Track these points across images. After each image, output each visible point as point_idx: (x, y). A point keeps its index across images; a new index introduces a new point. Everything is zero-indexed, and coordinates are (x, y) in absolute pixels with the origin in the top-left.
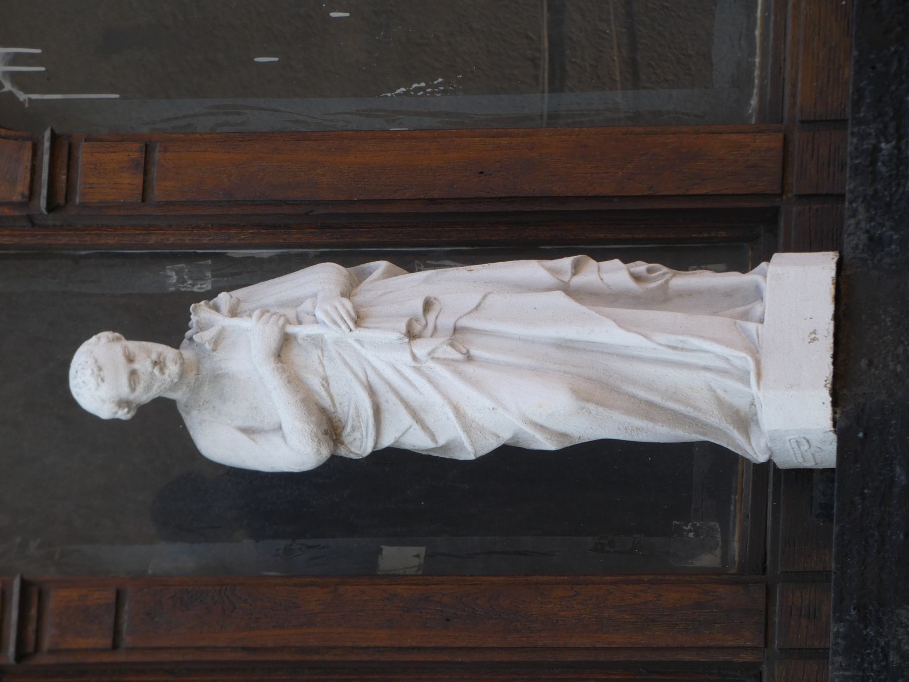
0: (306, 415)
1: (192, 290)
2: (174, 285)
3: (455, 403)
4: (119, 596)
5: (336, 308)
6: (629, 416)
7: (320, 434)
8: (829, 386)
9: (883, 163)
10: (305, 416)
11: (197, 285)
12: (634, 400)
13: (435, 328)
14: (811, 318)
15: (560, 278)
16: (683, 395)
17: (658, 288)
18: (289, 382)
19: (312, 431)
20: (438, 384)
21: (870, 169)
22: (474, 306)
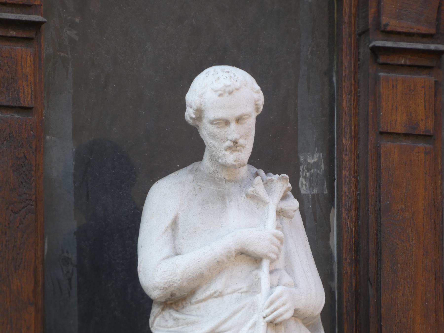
1: (301, 176)
2: (305, 160)
4: (27, 109)
5: (284, 304)
7: (170, 290)
11: (305, 181)
18: (218, 262)
19: (174, 282)
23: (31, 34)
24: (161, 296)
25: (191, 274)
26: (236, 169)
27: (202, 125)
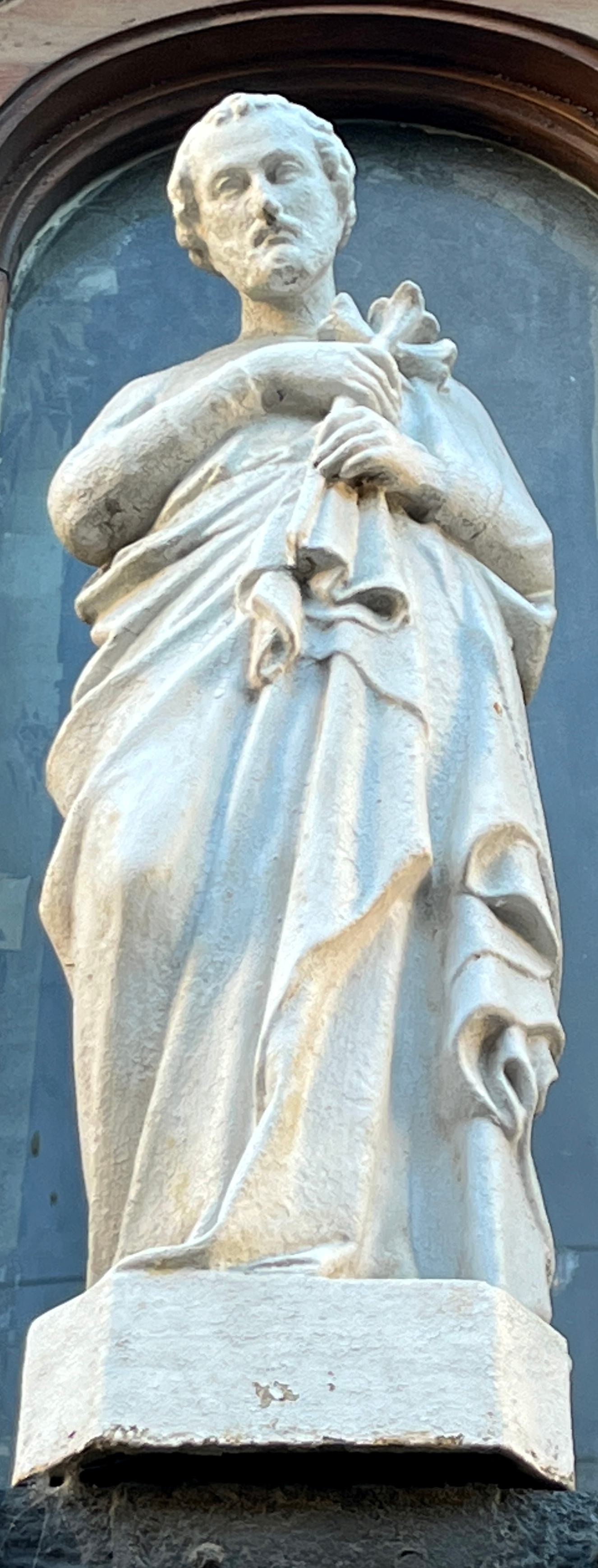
0: (141, 450)
3: (140, 678)
6: (105, 1037)
7: (100, 492)
8: (118, 1436)
10: (138, 447)
12: (152, 1050)
13: (330, 624)
14: (332, 1387)
16: (168, 1164)
17: (474, 1095)
19: (106, 469)
20: (190, 640)
22: (384, 686)
25: (146, 443)
26: (548, 985)
27: (268, 382)
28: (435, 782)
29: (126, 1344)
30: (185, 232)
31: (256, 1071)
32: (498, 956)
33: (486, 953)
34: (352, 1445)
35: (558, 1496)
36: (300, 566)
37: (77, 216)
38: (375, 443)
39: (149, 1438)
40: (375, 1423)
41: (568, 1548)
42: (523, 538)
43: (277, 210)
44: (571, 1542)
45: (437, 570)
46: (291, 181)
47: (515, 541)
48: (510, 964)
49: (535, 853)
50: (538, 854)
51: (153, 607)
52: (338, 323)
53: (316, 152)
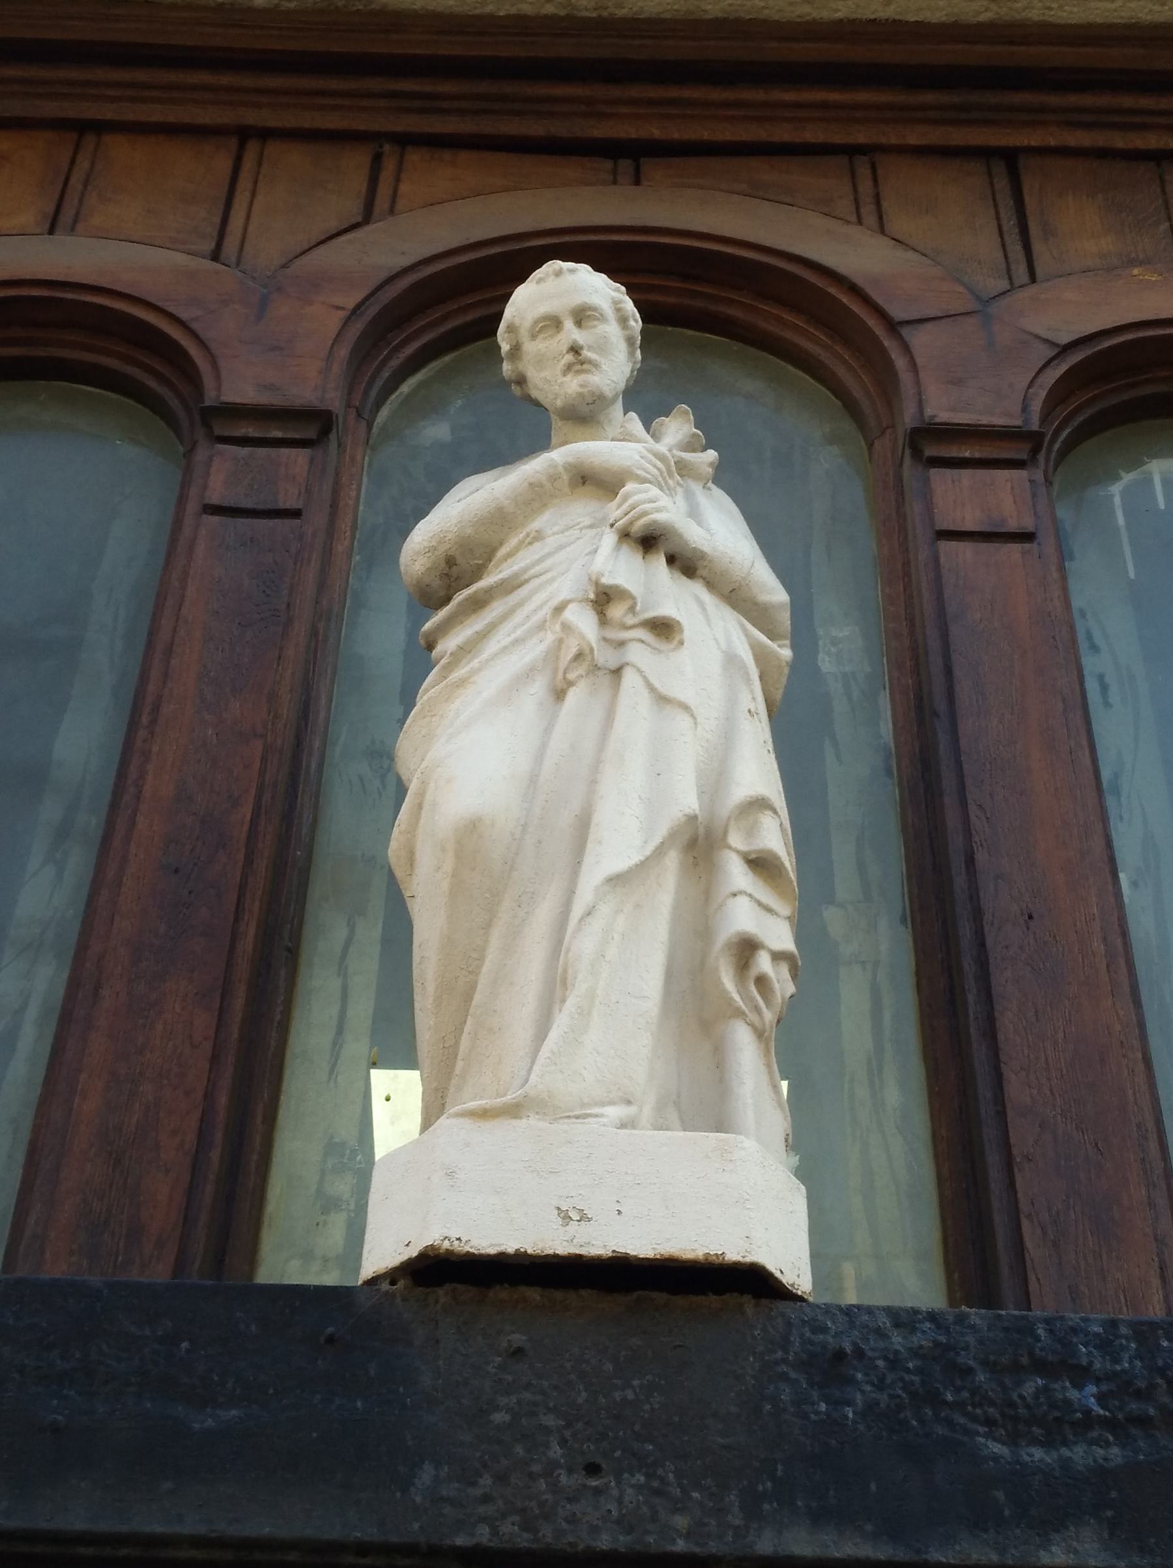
0: (474, 518)
3: (472, 680)
4: (296, 514)
7: (442, 549)
8: (446, 1244)
9: (1046, 1389)
13: (621, 644)
14: (619, 1212)
15: (732, 823)
17: (730, 1001)
19: (446, 532)
21: (1025, 1360)
22: (664, 691)
23: (311, 433)
24: (427, 567)
25: (478, 512)
28: (701, 764)
29: (454, 1174)
30: (510, 367)
31: (560, 970)
32: (750, 896)
33: (742, 892)
34: (636, 1258)
35: (801, 1306)
36: (598, 599)
37: (421, 385)
38: (658, 510)
39: (471, 1248)
40: (654, 1241)
41: (809, 1347)
42: (769, 596)
43: (581, 348)
44: (812, 1343)
45: (704, 609)
46: (595, 327)
47: (763, 598)
48: (760, 904)
49: (779, 823)
50: (781, 825)
51: (482, 631)
52: (627, 435)
53: (613, 308)
